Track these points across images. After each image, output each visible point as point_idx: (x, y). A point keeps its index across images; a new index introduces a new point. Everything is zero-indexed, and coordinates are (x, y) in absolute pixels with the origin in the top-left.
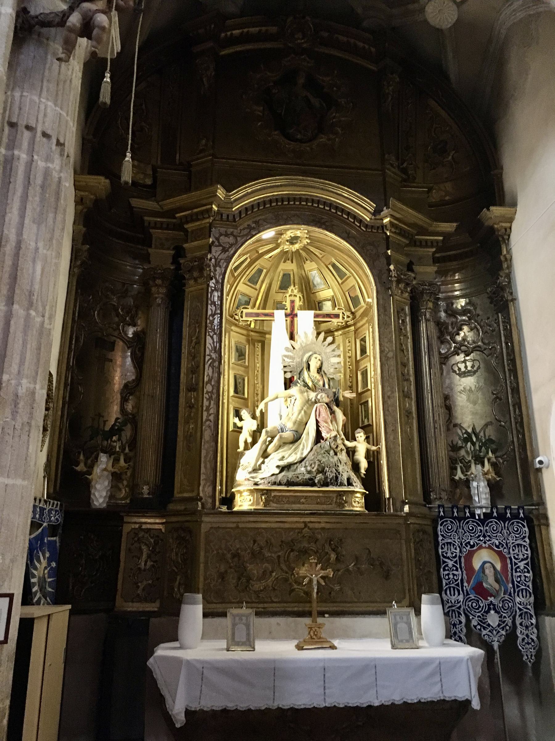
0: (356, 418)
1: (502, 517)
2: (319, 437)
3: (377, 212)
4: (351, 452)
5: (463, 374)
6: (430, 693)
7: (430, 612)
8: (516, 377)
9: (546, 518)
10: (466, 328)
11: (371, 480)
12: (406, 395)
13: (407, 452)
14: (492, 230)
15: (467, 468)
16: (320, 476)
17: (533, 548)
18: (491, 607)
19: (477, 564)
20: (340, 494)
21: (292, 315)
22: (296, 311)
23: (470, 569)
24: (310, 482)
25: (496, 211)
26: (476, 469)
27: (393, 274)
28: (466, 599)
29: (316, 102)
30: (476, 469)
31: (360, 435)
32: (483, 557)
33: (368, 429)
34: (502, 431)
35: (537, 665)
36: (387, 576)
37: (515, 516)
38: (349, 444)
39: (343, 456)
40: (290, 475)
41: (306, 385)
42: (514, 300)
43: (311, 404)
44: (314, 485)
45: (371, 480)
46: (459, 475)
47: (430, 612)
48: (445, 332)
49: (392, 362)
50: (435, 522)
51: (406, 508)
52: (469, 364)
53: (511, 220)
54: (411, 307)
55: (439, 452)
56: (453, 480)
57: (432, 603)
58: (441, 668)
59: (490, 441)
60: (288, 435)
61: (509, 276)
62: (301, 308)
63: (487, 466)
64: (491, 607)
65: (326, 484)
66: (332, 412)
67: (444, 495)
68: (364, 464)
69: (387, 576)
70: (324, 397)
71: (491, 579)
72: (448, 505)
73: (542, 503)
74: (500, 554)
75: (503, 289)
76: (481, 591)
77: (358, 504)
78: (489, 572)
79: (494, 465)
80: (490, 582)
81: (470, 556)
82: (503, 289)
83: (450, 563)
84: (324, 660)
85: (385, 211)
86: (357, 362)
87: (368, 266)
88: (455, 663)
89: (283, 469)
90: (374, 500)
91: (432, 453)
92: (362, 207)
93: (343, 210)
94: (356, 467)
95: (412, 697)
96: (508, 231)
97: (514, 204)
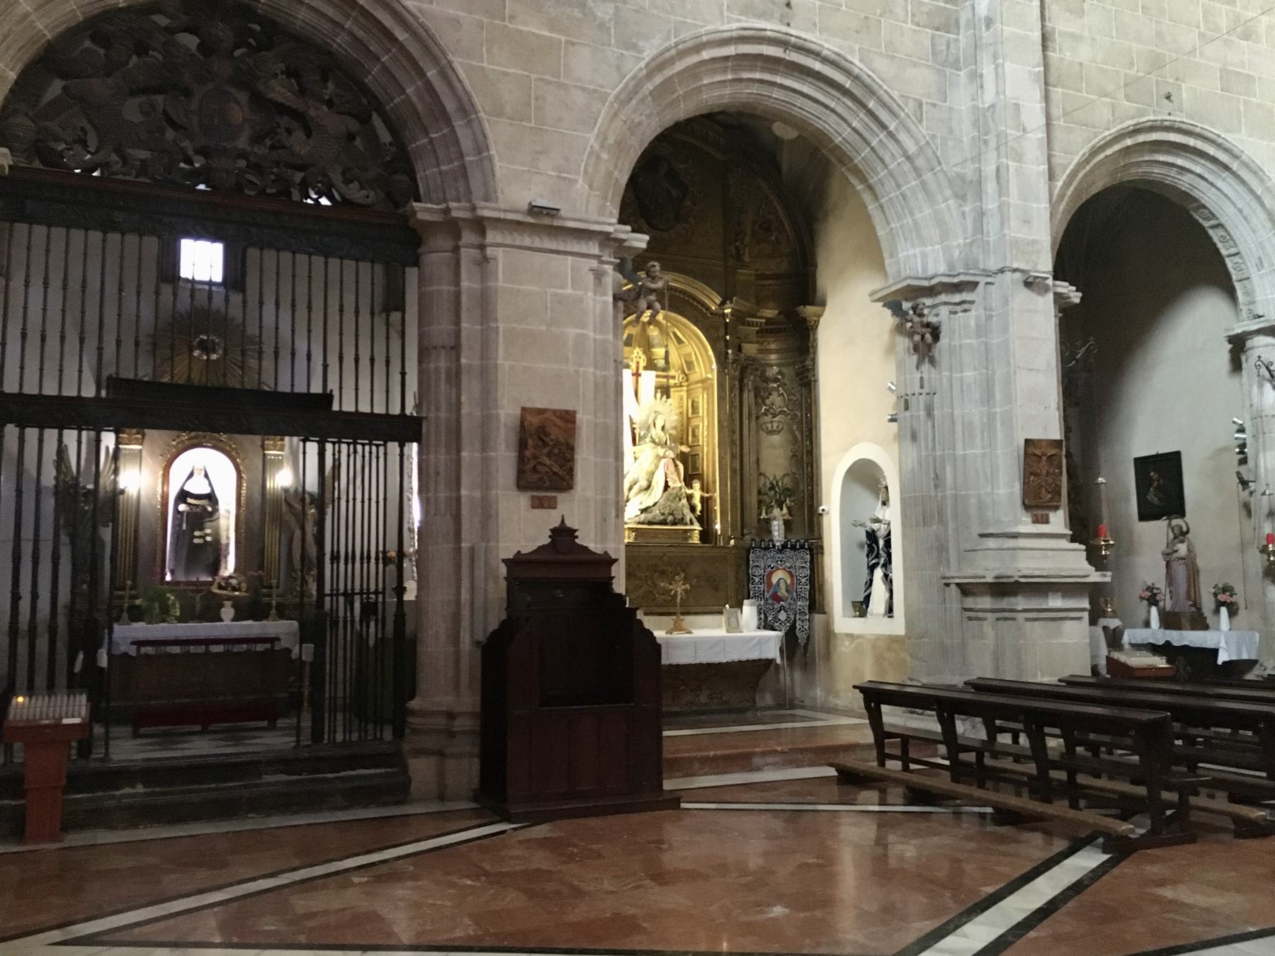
0: (691, 468)
1: (793, 548)
2: (666, 487)
3: (723, 304)
4: (690, 497)
5: (771, 432)
6: (754, 656)
7: (749, 611)
8: (811, 443)
9: (822, 548)
10: (775, 394)
11: (705, 518)
12: (733, 456)
13: (733, 501)
14: (804, 320)
15: (769, 508)
16: (670, 518)
17: (812, 570)
18: (782, 608)
19: (774, 580)
20: (686, 531)
21: (637, 375)
22: (641, 371)
23: (770, 584)
24: (664, 522)
25: (810, 310)
26: (776, 511)
27: (730, 357)
28: (766, 603)
29: (674, 193)
30: (776, 511)
31: (697, 485)
32: (778, 576)
33: (700, 477)
34: (796, 482)
35: (806, 645)
36: (716, 589)
37: (802, 547)
38: (689, 492)
39: (684, 501)
40: (649, 516)
41: (653, 441)
42: (816, 381)
43: (659, 458)
44: (666, 524)
45: (705, 518)
46: (763, 516)
47: (749, 611)
48: (761, 395)
49: (726, 430)
50: (748, 552)
51: (732, 542)
52: (775, 425)
53: (820, 316)
54: (740, 378)
55: (752, 499)
56: (759, 520)
57: (752, 605)
58: (761, 642)
59: (788, 489)
60: (644, 483)
61: (814, 360)
62: (646, 368)
63: (785, 510)
64: (782, 608)
65: (675, 524)
66: (676, 466)
67: (754, 531)
68: (699, 507)
69: (716, 589)
70: (671, 454)
71: (783, 590)
72: (758, 539)
73: (820, 538)
74: (790, 573)
75: (808, 370)
76: (776, 598)
77: (696, 539)
78: (782, 585)
79: (788, 508)
80: (782, 592)
81: (770, 574)
82: (808, 370)
83: (757, 580)
84: (905, 569)
85: (728, 304)
86: (688, 419)
87: (689, 319)
88: (770, 638)
89: (643, 511)
90: (707, 535)
91: (747, 498)
92: (712, 301)
93: (694, 299)
94: (693, 509)
95: (744, 657)
96: (817, 322)
97: (823, 304)
